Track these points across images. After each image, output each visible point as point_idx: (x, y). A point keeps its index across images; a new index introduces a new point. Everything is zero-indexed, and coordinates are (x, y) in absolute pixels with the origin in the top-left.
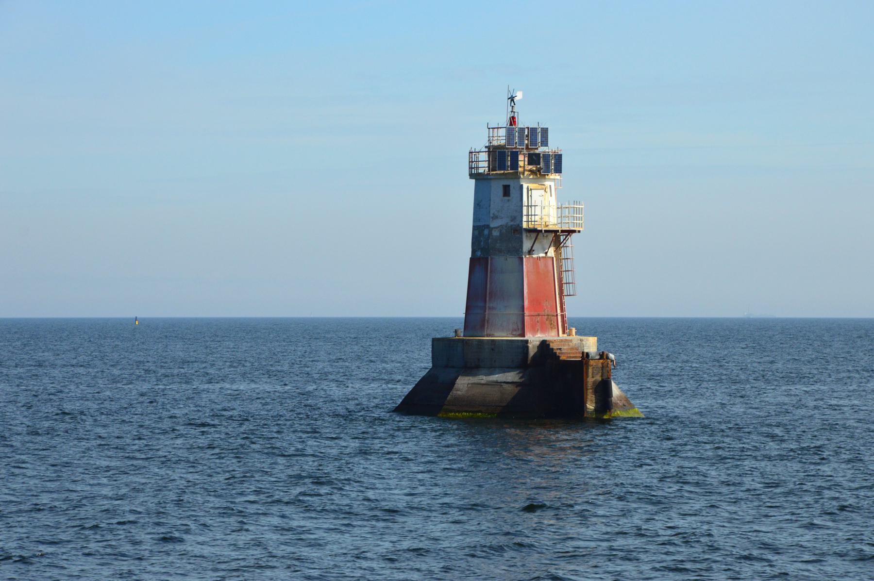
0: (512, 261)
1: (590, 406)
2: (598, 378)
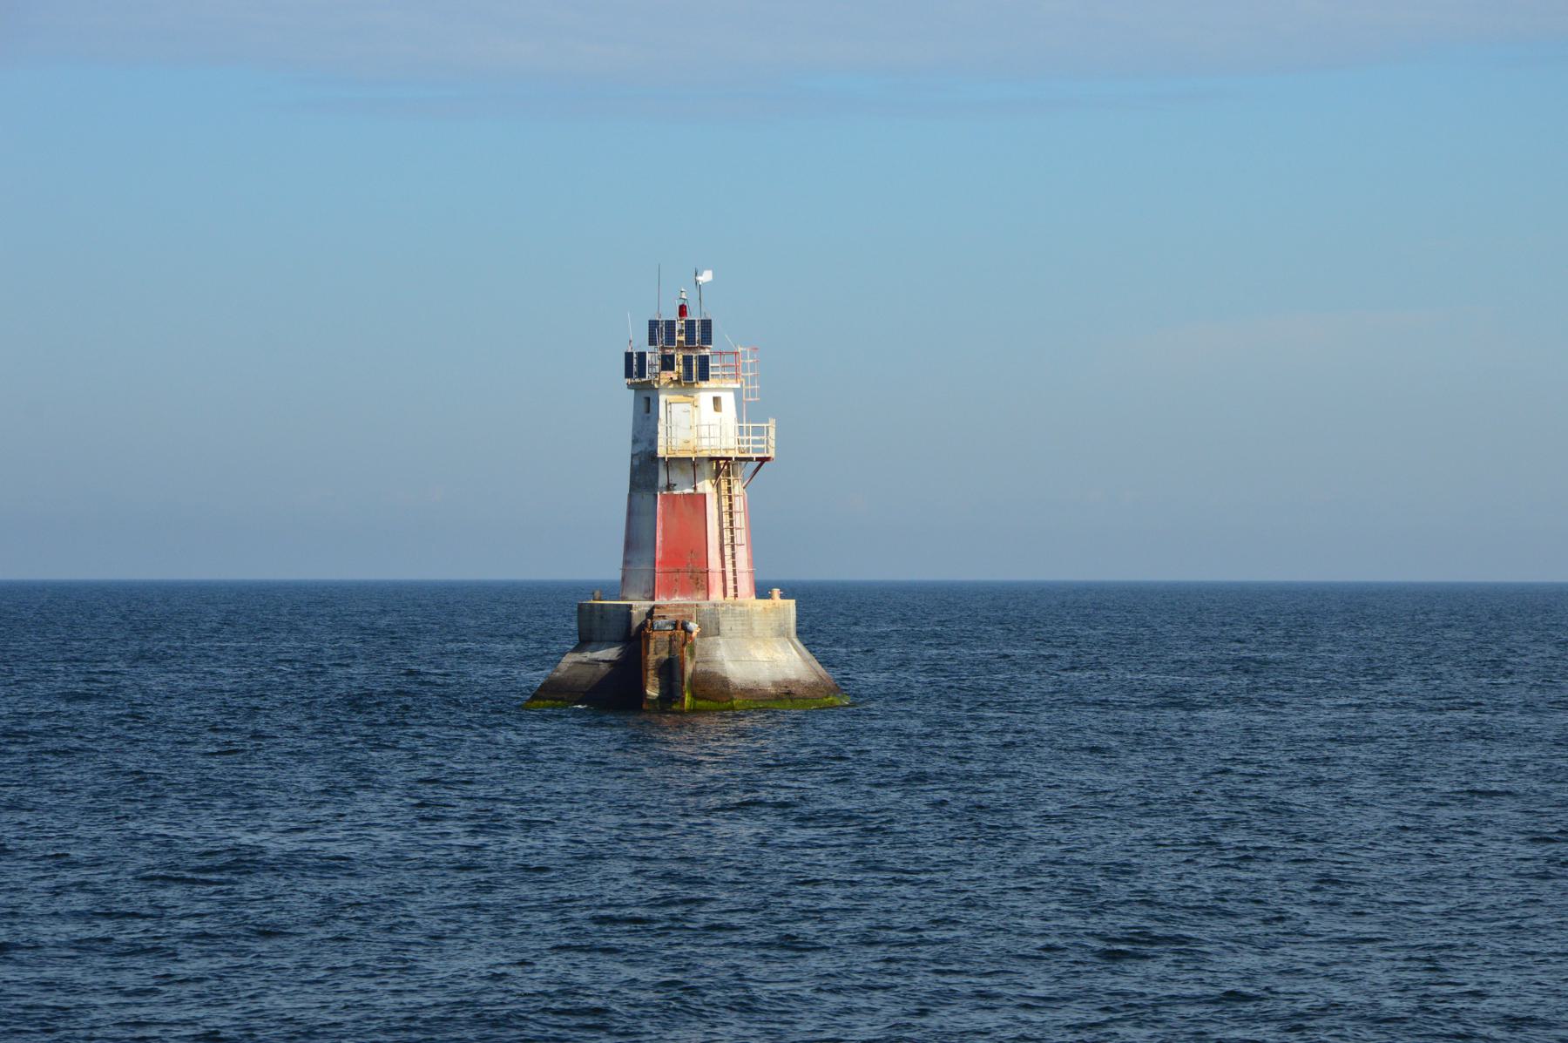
0: (648, 497)
1: (652, 692)
2: (665, 655)
